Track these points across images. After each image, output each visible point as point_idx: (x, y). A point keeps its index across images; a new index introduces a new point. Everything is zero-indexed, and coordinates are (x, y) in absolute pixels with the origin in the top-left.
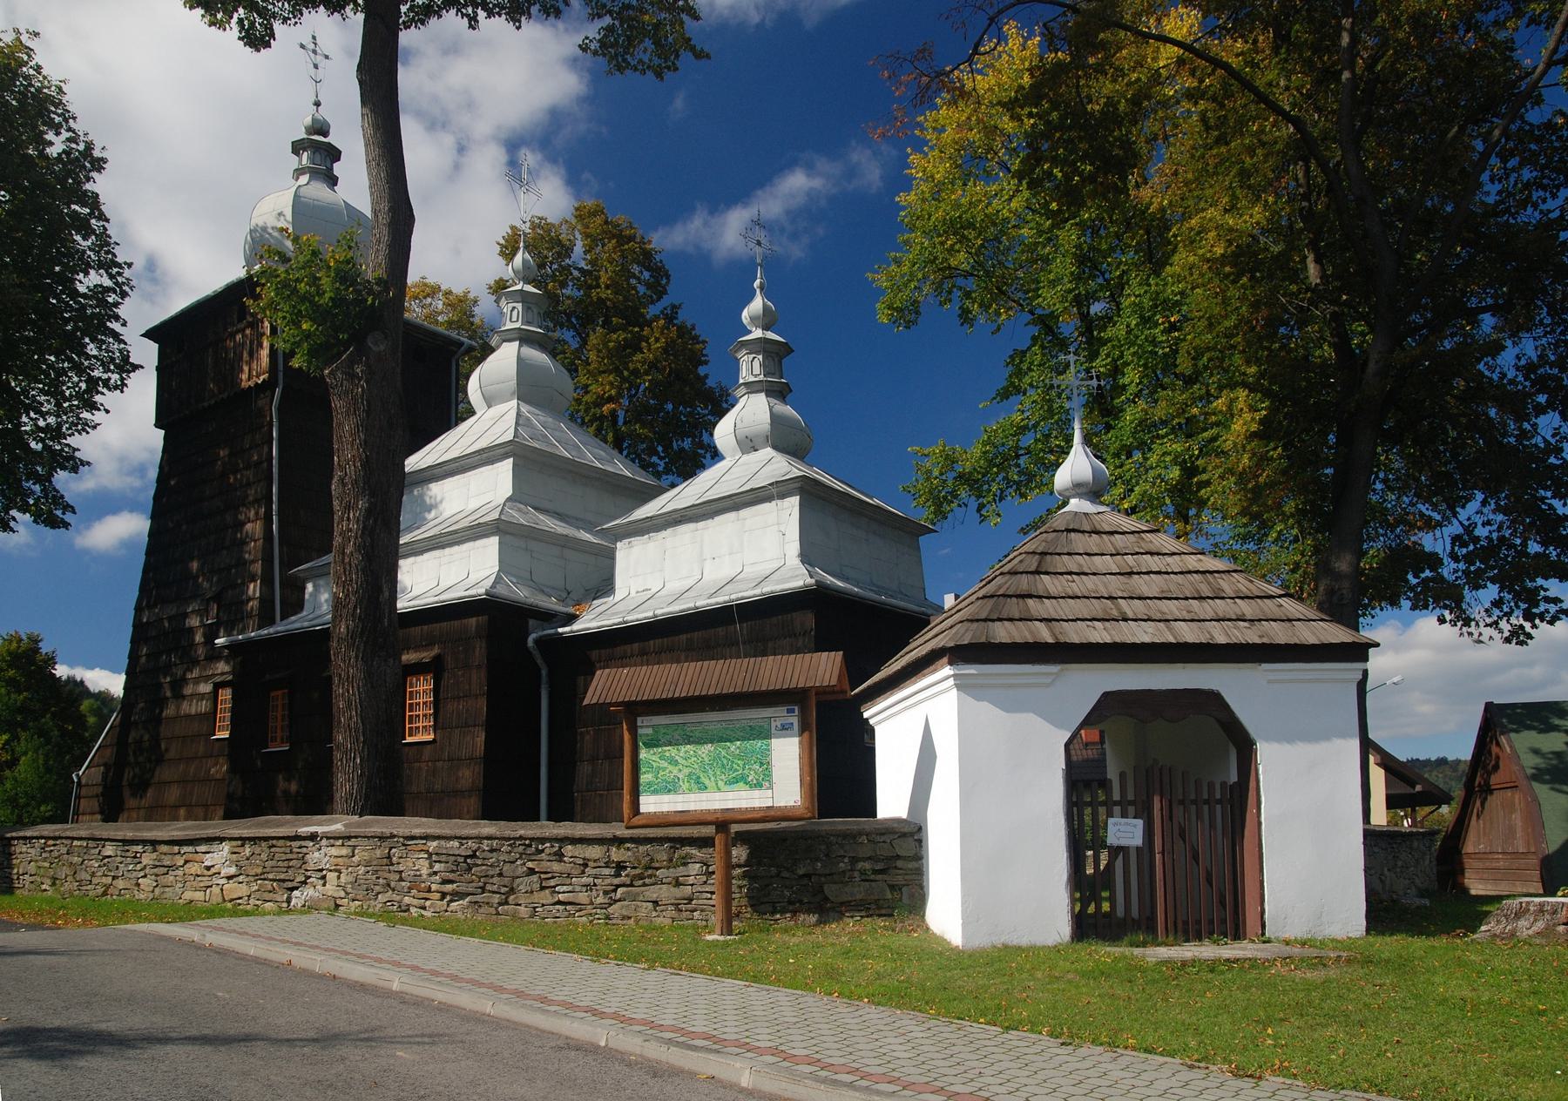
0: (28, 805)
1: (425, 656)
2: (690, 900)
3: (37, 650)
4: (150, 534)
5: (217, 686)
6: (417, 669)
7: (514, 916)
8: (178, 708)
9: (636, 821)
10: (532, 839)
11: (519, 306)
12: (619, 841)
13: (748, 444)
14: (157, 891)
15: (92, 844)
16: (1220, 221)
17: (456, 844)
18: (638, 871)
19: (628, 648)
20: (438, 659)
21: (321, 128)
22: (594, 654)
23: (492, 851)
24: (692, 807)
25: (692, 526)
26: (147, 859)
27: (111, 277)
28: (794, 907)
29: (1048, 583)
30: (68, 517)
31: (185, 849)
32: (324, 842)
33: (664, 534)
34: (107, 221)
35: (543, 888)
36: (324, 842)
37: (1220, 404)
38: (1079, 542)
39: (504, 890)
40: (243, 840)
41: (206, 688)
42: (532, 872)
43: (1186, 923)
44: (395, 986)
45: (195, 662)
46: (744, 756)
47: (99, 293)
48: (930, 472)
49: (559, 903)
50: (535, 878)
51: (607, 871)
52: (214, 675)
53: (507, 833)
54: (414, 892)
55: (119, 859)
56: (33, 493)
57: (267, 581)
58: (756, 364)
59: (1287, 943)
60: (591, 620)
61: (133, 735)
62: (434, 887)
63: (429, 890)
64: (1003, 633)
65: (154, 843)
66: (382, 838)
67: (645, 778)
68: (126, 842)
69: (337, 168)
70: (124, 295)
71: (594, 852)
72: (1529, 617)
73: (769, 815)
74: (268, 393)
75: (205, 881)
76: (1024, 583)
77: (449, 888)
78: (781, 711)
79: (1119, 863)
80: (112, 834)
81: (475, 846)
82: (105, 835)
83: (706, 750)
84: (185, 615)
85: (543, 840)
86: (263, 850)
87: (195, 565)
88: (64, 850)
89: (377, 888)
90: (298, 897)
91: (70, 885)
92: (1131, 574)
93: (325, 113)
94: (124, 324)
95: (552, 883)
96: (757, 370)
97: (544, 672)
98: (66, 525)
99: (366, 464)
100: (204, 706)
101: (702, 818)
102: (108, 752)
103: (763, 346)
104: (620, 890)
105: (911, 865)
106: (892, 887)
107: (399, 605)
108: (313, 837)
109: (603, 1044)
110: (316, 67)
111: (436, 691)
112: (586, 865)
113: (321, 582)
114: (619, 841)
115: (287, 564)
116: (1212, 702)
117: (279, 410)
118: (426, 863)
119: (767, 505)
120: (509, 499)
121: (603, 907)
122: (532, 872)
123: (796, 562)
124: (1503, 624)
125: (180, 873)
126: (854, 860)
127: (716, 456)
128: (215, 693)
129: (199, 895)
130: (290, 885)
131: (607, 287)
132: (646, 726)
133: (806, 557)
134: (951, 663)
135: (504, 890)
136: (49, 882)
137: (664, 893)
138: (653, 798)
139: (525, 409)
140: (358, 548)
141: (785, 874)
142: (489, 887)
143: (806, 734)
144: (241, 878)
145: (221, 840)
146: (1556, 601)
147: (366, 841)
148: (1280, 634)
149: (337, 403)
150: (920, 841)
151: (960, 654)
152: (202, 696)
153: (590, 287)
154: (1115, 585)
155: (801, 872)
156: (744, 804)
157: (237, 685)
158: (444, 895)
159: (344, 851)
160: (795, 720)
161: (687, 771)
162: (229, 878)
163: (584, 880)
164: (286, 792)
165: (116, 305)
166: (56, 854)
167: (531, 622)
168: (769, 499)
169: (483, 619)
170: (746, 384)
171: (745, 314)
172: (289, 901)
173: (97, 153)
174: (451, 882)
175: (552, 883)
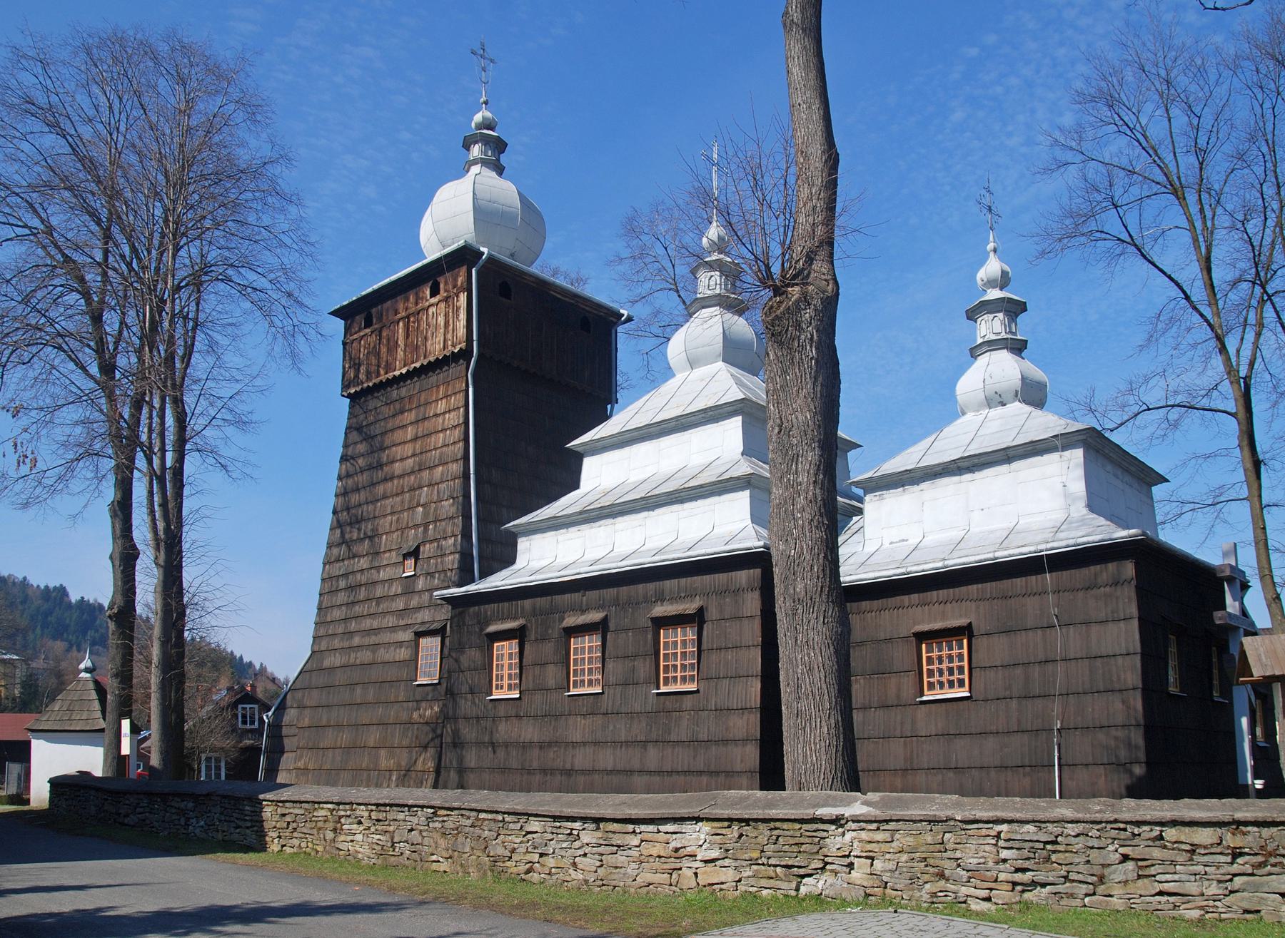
17: (1030, 828)
19: (906, 599)
20: (701, 610)
26: (586, 837)
31: (643, 828)
35: (1139, 877)
40: (730, 820)
42: (1125, 858)
49: (1161, 893)
50: (1130, 865)
51: (1222, 859)
62: (1002, 877)
66: (933, 821)
71: (1204, 836)
89: (926, 877)
95: (1152, 871)
100: (403, 654)
104: (1238, 881)
108: (837, 821)
117: (474, 376)
122: (1125, 858)
123: (1085, 511)
125: (635, 853)
130: (802, 871)
144: (726, 862)
152: (400, 644)
172: (797, 889)
174: (1024, 870)
175: (1152, 871)
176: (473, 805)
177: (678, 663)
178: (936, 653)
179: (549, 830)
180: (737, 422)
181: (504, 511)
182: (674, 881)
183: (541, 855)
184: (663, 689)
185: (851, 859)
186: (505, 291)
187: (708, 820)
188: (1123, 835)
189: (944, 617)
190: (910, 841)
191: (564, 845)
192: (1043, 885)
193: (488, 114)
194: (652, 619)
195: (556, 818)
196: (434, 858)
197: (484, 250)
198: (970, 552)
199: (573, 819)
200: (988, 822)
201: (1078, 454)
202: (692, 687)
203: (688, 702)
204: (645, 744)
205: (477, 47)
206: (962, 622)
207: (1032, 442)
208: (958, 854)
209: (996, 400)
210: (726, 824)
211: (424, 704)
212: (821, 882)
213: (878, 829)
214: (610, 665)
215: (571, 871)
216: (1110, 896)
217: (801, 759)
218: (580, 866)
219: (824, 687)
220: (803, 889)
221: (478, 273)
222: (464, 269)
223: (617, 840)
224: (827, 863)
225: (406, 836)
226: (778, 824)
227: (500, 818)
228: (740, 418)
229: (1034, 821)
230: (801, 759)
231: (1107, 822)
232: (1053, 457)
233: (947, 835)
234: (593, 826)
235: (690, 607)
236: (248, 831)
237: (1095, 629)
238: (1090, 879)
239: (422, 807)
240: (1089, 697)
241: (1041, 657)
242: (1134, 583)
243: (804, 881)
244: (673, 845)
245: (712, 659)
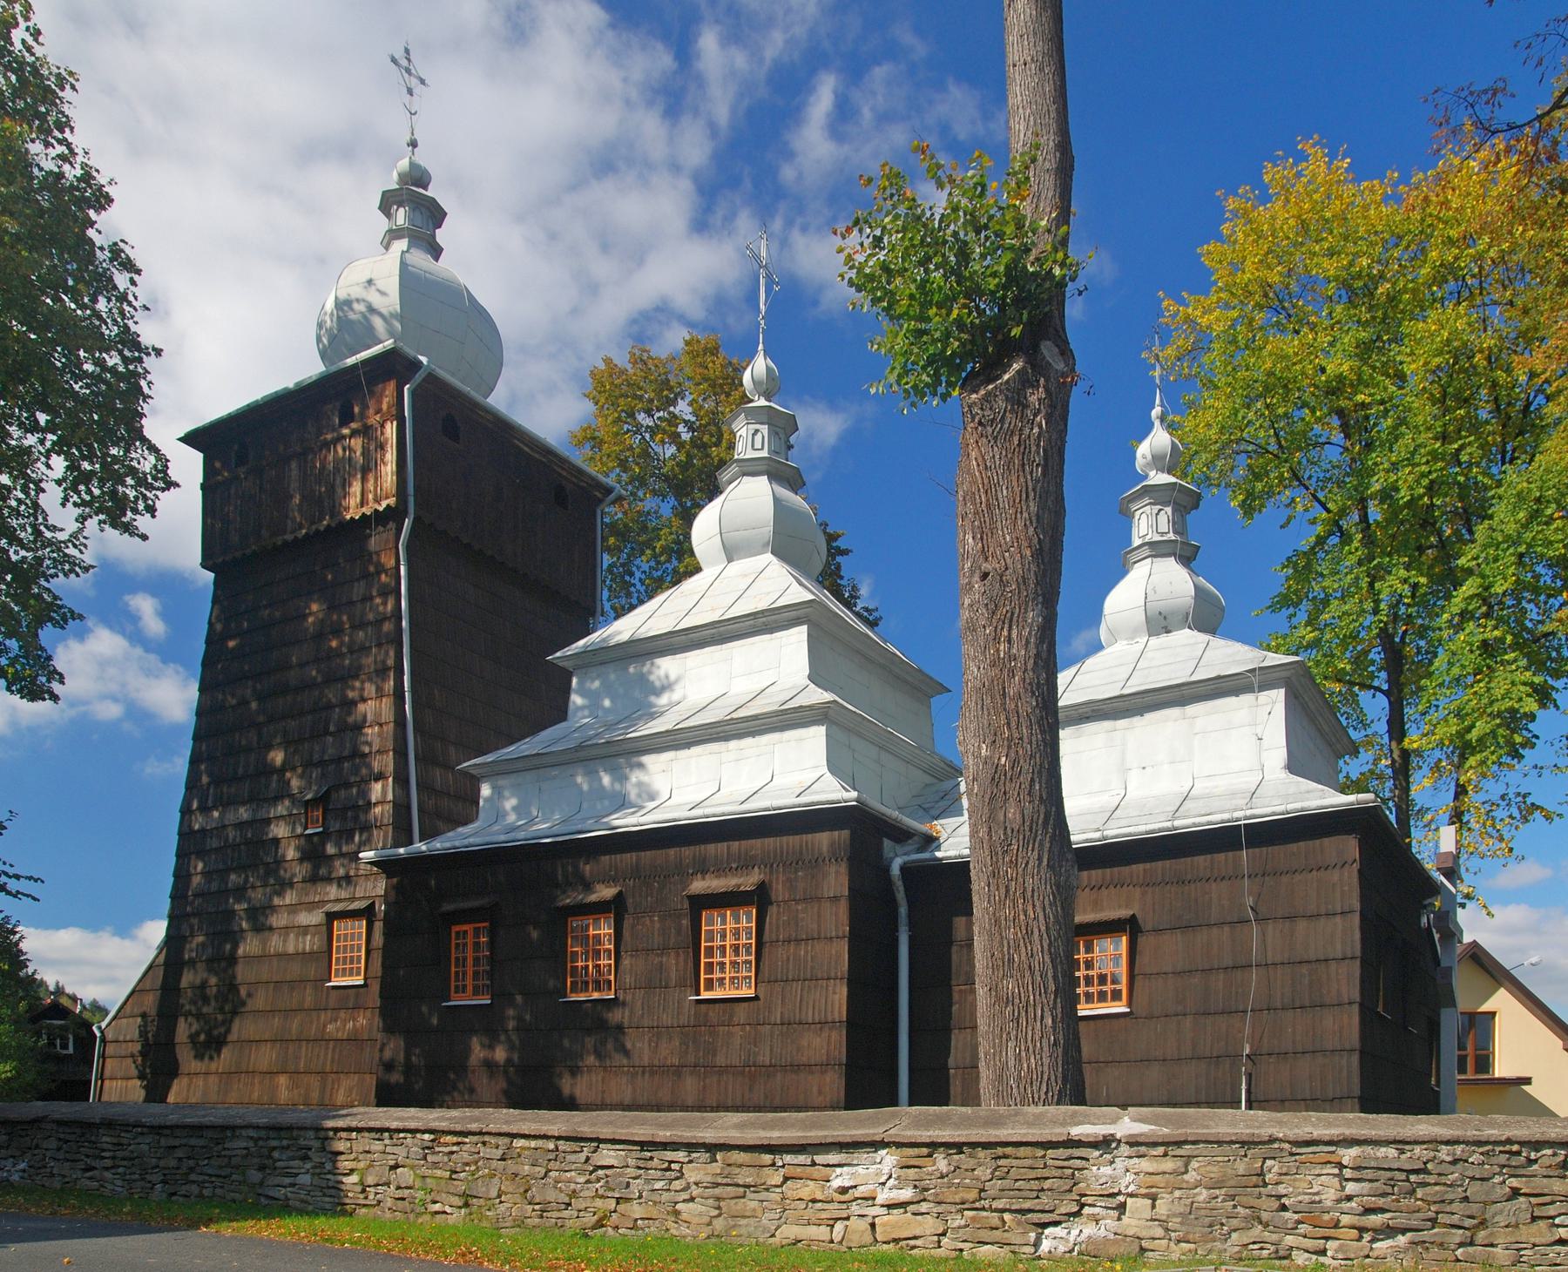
1: (606, 892)
4: (200, 713)
5: (331, 917)
6: (600, 908)
8: (264, 943)
11: (764, 429)
15: (562, 1145)
17: (1391, 1152)
21: (417, 177)
23: (1455, 1162)
25: (1107, 724)
31: (788, 1158)
34: (139, 272)
35: (1534, 1219)
39: (1468, 1223)
40: (933, 1146)
42: (1516, 1193)
45: (284, 885)
55: (631, 1171)
57: (401, 780)
58: (1163, 518)
61: (187, 979)
62: (1345, 1220)
63: (1336, 1225)
69: (441, 236)
74: (392, 525)
75: (833, 1210)
77: (1376, 1220)
82: (606, 1132)
85: (1537, 1145)
87: (278, 757)
89: (1235, 1223)
91: (511, 1207)
93: (423, 158)
95: (1551, 1210)
96: (1164, 527)
97: (903, 911)
100: (309, 943)
103: (1158, 495)
108: (1105, 1144)
110: (410, 92)
113: (502, 782)
117: (408, 548)
122: (1516, 1193)
125: (775, 1196)
144: (924, 1207)
152: (305, 930)
159: (1169, 1165)
164: (489, 1065)
168: (1236, 692)
170: (1151, 544)
172: (1037, 1244)
175: (1551, 1210)
176: (505, 1129)
177: (727, 960)
179: (631, 1162)
180: (799, 634)
181: (452, 750)
182: (837, 1236)
183: (618, 1200)
184: (705, 995)
185: (1121, 1198)
186: (451, 429)
187: (899, 1145)
188: (1515, 1161)
190: (1215, 1171)
191: (659, 1185)
192: (1404, 1231)
194: (689, 897)
195: (644, 1145)
196: (437, 1207)
197: (424, 360)
198: (1134, 821)
199: (665, 1146)
200: (1329, 1143)
201: (1276, 699)
202: (748, 992)
203: (741, 1012)
204: (678, 1071)
205: (400, 54)
206: (1124, 913)
207: (1219, 677)
208: (1281, 1189)
209: (1159, 623)
210: (925, 1151)
211: (342, 1014)
212: (1075, 1232)
213: (1165, 1155)
214: (626, 962)
215: (670, 1224)
216: (1492, 1245)
217: (1011, 1063)
218: (684, 1216)
219: (1047, 958)
220: (1046, 1245)
221: (413, 393)
222: (391, 388)
223: (745, 1177)
224: (1083, 1206)
225: (387, 1175)
226: (1009, 1150)
227: (551, 1146)
228: (804, 628)
229: (1395, 1142)
230: (1011, 1063)
231: (1496, 1143)
232: (1246, 699)
233: (1269, 1163)
235: (747, 881)
236: (108, 1175)
237: (1302, 925)
238: (1468, 1223)
239: (414, 1131)
240: (1290, 1014)
241: (1228, 962)
242: (1356, 866)
243: (1047, 1231)
244: (836, 1183)
245: (778, 956)
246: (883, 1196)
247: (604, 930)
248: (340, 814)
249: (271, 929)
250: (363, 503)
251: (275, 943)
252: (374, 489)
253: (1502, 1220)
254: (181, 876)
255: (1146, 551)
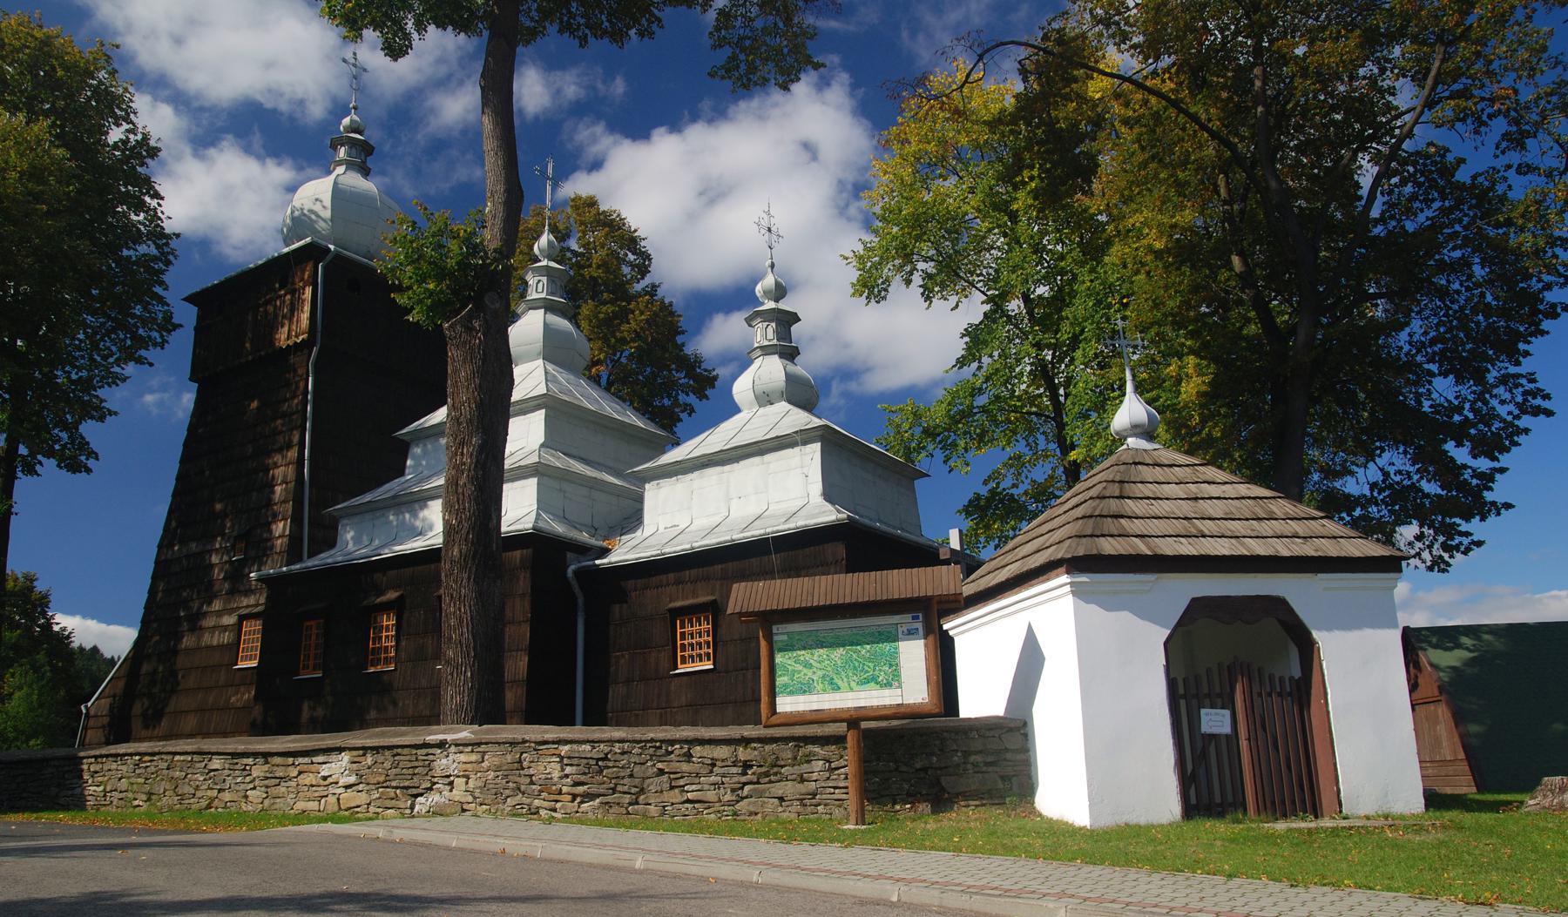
0: (16, 739)
1: (392, 595)
2: (814, 795)
3: (31, 589)
5: (242, 618)
6: (387, 607)
7: (645, 815)
9: (774, 720)
10: (662, 741)
11: (545, 279)
12: (745, 741)
13: (765, 399)
14: (267, 802)
15: (196, 758)
16: (1150, 225)
17: (588, 747)
18: (763, 769)
19: (664, 577)
22: (630, 584)
23: (623, 753)
24: (826, 706)
25: (718, 469)
26: (257, 772)
27: (158, 247)
28: (913, 797)
29: (1131, 506)
30: (91, 463)
31: (301, 760)
32: (453, 749)
33: (690, 476)
35: (672, 788)
36: (453, 749)
37: (1172, 369)
38: (1147, 473)
39: (634, 790)
40: (365, 749)
41: (229, 620)
42: (661, 772)
43: (1273, 803)
44: (638, 864)
46: (874, 658)
47: (145, 261)
48: (899, 426)
49: (688, 801)
51: (734, 770)
52: (239, 608)
53: (638, 736)
54: (544, 795)
55: (226, 772)
56: (60, 439)
57: (297, 520)
58: (770, 330)
59: (1368, 818)
60: (625, 552)
61: (146, 668)
62: (565, 789)
63: (560, 793)
64: (1109, 547)
65: (266, 755)
66: (513, 744)
67: (780, 681)
68: (234, 755)
70: (168, 263)
71: (722, 752)
72: (1445, 547)
73: (900, 712)
75: (321, 791)
76: (1113, 506)
77: (580, 789)
78: (908, 617)
79: (1212, 749)
80: (221, 748)
81: (607, 749)
82: (214, 749)
83: (838, 654)
84: (210, 552)
85: (672, 742)
86: (387, 759)
88: (164, 765)
89: (507, 792)
90: (422, 804)
91: (170, 800)
92: (1196, 499)
94: (166, 289)
95: (682, 782)
96: (770, 334)
97: (581, 600)
98: (89, 471)
99: (480, 406)
100: (226, 638)
101: (809, 718)
102: (121, 684)
104: (747, 788)
105: (1020, 757)
106: (1003, 778)
107: (504, 529)
108: (442, 745)
109: (895, 899)
111: (399, 626)
112: (714, 765)
114: (745, 741)
115: (319, 504)
116: (1278, 607)
118: (558, 766)
119: (789, 451)
120: (542, 446)
121: (730, 804)
122: (661, 772)
123: (820, 500)
124: (1426, 555)
125: (293, 784)
126: (967, 754)
127: (736, 410)
128: (239, 625)
129: (313, 805)
130: (415, 791)
131: (598, 267)
132: (782, 632)
133: (829, 495)
134: (1068, 573)
135: (634, 790)
136: (144, 797)
137: (788, 789)
138: (789, 699)
139: (550, 367)
140: (471, 480)
141: (903, 768)
142: (619, 788)
143: (931, 638)
144: (361, 787)
145: (340, 750)
146: (1467, 534)
147: (496, 747)
148: (1331, 549)
149: (452, 352)
150: (1026, 736)
151: (1075, 565)
152: (225, 628)
153: (583, 267)
154: (1186, 508)
155: (918, 766)
156: (875, 702)
157: (268, 617)
158: (574, 797)
159: (474, 757)
160: (919, 626)
161: (820, 673)
162: (347, 787)
163: (713, 779)
165: (162, 272)
166: (153, 769)
167: (569, 555)
168: (792, 445)
169: (527, 552)
170: (761, 348)
171: (759, 288)
172: (412, 808)
173: (152, 143)
175: (682, 782)
178: (688, 629)
187: (351, 749)
189: (695, 595)
190: (496, 761)
193: (356, 118)
197: (332, 247)
201: (815, 448)
209: (765, 399)
221: (324, 268)
222: (309, 267)
234: (261, 760)
246: (343, 781)
247: (388, 621)
248: (254, 544)
249: (201, 628)
250: (289, 337)
251: (207, 639)
252: (296, 327)
253: (653, 788)
254: (152, 592)
255: (758, 352)
